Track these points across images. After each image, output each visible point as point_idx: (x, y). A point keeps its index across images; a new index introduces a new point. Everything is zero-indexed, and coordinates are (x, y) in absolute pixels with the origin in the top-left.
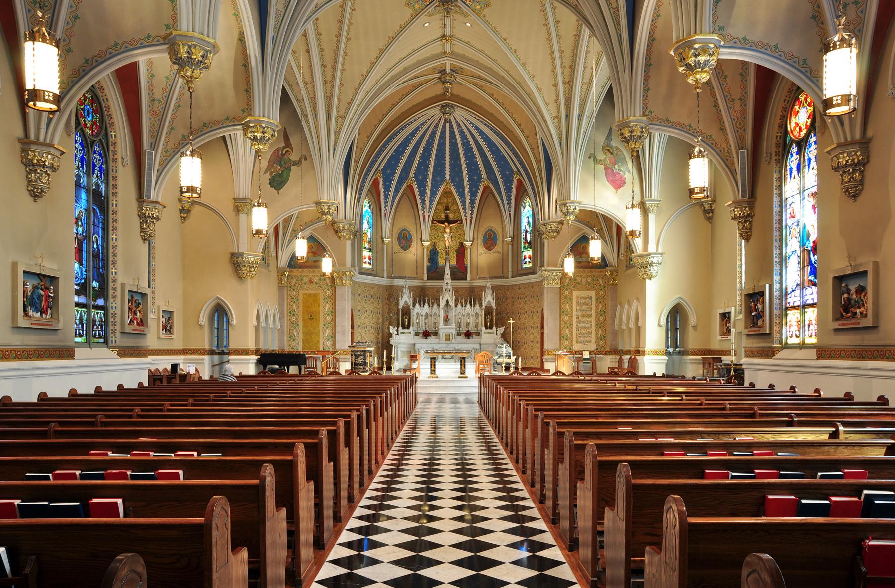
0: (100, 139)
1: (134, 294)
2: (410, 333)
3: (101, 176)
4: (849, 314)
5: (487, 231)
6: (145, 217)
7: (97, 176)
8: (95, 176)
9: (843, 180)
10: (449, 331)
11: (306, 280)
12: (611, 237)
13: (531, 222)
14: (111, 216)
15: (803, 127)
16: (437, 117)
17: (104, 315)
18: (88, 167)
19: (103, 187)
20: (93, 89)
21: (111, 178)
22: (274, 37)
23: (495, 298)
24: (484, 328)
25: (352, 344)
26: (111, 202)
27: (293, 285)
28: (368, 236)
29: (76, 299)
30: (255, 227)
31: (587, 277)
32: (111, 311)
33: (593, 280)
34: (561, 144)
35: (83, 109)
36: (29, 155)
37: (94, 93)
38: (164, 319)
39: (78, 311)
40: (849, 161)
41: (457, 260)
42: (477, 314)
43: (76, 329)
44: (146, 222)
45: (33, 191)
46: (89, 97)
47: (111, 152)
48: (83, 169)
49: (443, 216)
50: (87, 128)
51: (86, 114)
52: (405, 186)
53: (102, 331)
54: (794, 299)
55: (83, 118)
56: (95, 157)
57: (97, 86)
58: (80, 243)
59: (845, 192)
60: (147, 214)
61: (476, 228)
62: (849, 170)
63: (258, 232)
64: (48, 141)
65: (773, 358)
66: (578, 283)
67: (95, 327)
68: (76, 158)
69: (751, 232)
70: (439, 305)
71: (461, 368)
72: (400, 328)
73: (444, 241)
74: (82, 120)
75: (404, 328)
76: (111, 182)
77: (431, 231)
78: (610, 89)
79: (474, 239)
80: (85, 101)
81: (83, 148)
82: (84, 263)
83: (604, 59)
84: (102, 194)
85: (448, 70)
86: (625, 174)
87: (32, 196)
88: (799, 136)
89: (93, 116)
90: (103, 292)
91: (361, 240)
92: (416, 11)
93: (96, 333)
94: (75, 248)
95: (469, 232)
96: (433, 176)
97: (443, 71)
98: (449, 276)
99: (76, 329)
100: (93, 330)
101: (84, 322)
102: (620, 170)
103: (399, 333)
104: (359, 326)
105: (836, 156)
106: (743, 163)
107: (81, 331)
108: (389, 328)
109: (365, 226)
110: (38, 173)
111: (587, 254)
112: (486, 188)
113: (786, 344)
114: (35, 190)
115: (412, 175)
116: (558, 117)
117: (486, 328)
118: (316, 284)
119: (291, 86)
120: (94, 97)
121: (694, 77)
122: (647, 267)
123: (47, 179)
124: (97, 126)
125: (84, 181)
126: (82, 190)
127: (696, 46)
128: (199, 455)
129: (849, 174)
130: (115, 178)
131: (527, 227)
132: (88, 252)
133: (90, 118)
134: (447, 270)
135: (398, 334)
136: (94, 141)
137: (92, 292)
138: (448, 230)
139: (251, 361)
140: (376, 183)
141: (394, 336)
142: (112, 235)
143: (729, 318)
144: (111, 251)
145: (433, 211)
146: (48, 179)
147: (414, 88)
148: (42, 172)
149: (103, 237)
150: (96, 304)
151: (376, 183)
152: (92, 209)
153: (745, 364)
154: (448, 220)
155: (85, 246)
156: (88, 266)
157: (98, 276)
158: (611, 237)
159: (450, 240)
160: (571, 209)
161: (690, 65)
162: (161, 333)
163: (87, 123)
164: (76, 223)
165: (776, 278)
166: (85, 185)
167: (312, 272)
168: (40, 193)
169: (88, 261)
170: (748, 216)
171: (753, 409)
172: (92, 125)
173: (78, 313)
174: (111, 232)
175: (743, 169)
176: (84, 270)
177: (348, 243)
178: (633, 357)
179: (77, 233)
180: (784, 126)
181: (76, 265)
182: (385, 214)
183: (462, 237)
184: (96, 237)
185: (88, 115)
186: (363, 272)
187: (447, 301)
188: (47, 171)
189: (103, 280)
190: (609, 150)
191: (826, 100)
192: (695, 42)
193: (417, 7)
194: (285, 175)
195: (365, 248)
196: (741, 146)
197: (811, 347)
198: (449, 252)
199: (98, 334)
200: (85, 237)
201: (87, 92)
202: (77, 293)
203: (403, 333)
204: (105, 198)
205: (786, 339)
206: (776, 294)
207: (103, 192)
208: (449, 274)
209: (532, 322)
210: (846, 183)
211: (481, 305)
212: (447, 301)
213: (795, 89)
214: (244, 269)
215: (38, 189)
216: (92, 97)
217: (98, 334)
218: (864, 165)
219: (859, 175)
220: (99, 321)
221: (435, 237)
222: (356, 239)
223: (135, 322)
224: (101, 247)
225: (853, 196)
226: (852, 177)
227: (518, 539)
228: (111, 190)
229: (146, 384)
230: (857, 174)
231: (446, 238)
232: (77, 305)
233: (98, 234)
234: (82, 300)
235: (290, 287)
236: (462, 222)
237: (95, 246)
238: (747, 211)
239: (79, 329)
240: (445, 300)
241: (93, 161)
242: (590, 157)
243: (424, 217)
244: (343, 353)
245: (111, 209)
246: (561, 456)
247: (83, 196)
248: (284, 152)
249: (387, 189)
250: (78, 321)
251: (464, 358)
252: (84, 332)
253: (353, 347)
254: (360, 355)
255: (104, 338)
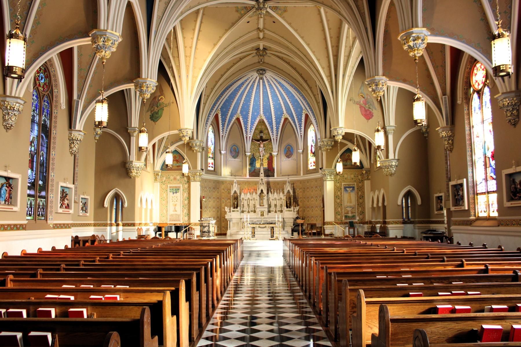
0: (48, 94)
1: (63, 188)
2: (238, 211)
3: (47, 115)
4: (516, 198)
5: (287, 146)
6: (73, 140)
7: (45, 116)
8: (44, 116)
9: (507, 115)
10: (263, 209)
11: (172, 178)
12: (365, 149)
13: (314, 140)
14: (52, 140)
15: (480, 83)
16: (255, 77)
17: (45, 202)
18: (40, 110)
19: (48, 122)
20: (45, 64)
21: (53, 117)
22: (155, 31)
23: (292, 189)
24: (286, 208)
25: (201, 219)
26: (52, 132)
27: (163, 181)
28: (211, 150)
29: (28, 192)
30: (98, 119)
31: (351, 174)
32: (49, 200)
33: (355, 176)
34: (332, 92)
35: (39, 76)
36: (5, 104)
37: (46, 66)
38: (82, 204)
39: (29, 199)
40: (510, 103)
41: (268, 165)
42: (281, 198)
43: (27, 211)
44: (73, 143)
45: (6, 126)
46: (43, 68)
47: (54, 101)
48: (36, 112)
49: (259, 137)
50: (41, 87)
51: (40, 78)
52: (235, 118)
53: (44, 212)
54: (481, 188)
55: (39, 81)
56: (44, 104)
57: (48, 64)
58: (32, 157)
59: (509, 122)
60: (74, 138)
61: (280, 144)
62: (510, 109)
63: (100, 123)
64: (17, 96)
65: (472, 225)
66: (346, 179)
67: (39, 209)
68: (33, 105)
69: (453, 146)
70: (256, 193)
71: (271, 234)
72: (232, 208)
73: (259, 152)
74: (38, 82)
75: (234, 208)
76: (53, 120)
77: (251, 146)
78: (362, 60)
79: (278, 151)
80: (40, 71)
81: (48, 105)
82: (34, 169)
83: (357, 42)
84: (47, 126)
85: (261, 48)
86: (372, 110)
87: (5, 129)
88: (478, 88)
89: (45, 80)
90: (45, 187)
91: (207, 152)
92: (242, 14)
93: (40, 213)
94: (29, 160)
95: (275, 147)
96: (252, 112)
97: (258, 49)
98: (263, 175)
99: (27, 211)
100: (38, 212)
101: (33, 206)
102: (369, 108)
103: (231, 211)
104: (206, 207)
105: (501, 100)
106: (446, 104)
107: (31, 212)
108: (224, 208)
109: (210, 143)
110: (10, 115)
111: (351, 160)
112: (286, 119)
113: (478, 217)
114: (8, 125)
115: (239, 112)
116: (330, 75)
117: (287, 207)
118: (178, 180)
119: (165, 59)
120: (46, 69)
121: (414, 53)
122: (388, 168)
123: (15, 118)
124: (46, 85)
125: (37, 119)
126: (35, 124)
127: (414, 35)
128: (115, 286)
129: (510, 111)
130: (56, 117)
131: (312, 143)
132: (37, 162)
133: (43, 81)
134: (262, 171)
135: (230, 212)
136: (44, 95)
137: (38, 187)
138: (262, 146)
139: (197, 229)
140: (216, 117)
141: (228, 213)
142: (52, 152)
143: (442, 200)
144: (51, 162)
145: (252, 133)
146: (16, 118)
147: (241, 59)
148: (12, 114)
149: (47, 153)
150: (41, 195)
151: (216, 117)
152: (41, 136)
153: (454, 230)
154: (262, 139)
155: (35, 158)
156: (37, 171)
157: (42, 177)
158: (365, 149)
159: (264, 152)
160: (340, 132)
161: (410, 46)
162: (80, 213)
163: (41, 84)
164: (31, 145)
165: (470, 174)
166: (38, 121)
167: (175, 173)
168: (10, 127)
169: (37, 168)
170: (450, 136)
171: (403, 250)
172: (44, 85)
173: (29, 200)
174: (51, 150)
175: (446, 107)
176: (34, 173)
177: (199, 155)
178: (374, 225)
179: (31, 151)
180: (468, 83)
181: (30, 171)
182: (222, 136)
183: (271, 150)
184: (42, 153)
185: (42, 79)
186: (208, 172)
187: (262, 191)
188: (15, 114)
189: (45, 179)
190: (362, 96)
191: (415, 120)
192: (412, 33)
193: (242, 12)
194: (160, 113)
195: (210, 157)
196: (444, 94)
197: (494, 219)
198: (263, 159)
199: (41, 214)
200: (36, 153)
201: (42, 66)
202: (29, 188)
203: (233, 211)
204: (49, 129)
205: (478, 213)
206: (470, 184)
207: (48, 126)
208: (263, 173)
209: (316, 203)
210: (509, 117)
211: (283, 193)
212: (262, 191)
213: (473, 61)
214: (133, 171)
215: (9, 124)
216: (45, 69)
217: (41, 214)
218: (453, 137)
219: (516, 111)
220: (42, 206)
221: (254, 150)
222: (204, 152)
223: (64, 206)
224: (45, 159)
225: (514, 125)
226: (512, 113)
227: (300, 321)
228: (53, 124)
229: (70, 246)
230: (515, 111)
231: (260, 151)
232: (29, 195)
233: (43, 151)
234: (32, 192)
235: (162, 182)
236: (271, 141)
237: (42, 159)
238: (450, 133)
239: (29, 211)
240: (260, 190)
241: (43, 107)
242: (350, 100)
243: (246, 137)
244: (195, 224)
245: (52, 136)
246: (340, 296)
247: (36, 128)
248: (160, 99)
249: (224, 120)
250: (29, 206)
251: (273, 228)
252: (33, 213)
253: (202, 221)
254: (206, 226)
255: (45, 217)
